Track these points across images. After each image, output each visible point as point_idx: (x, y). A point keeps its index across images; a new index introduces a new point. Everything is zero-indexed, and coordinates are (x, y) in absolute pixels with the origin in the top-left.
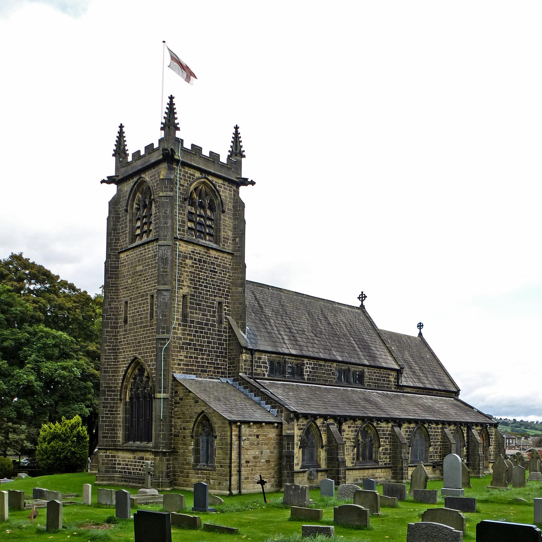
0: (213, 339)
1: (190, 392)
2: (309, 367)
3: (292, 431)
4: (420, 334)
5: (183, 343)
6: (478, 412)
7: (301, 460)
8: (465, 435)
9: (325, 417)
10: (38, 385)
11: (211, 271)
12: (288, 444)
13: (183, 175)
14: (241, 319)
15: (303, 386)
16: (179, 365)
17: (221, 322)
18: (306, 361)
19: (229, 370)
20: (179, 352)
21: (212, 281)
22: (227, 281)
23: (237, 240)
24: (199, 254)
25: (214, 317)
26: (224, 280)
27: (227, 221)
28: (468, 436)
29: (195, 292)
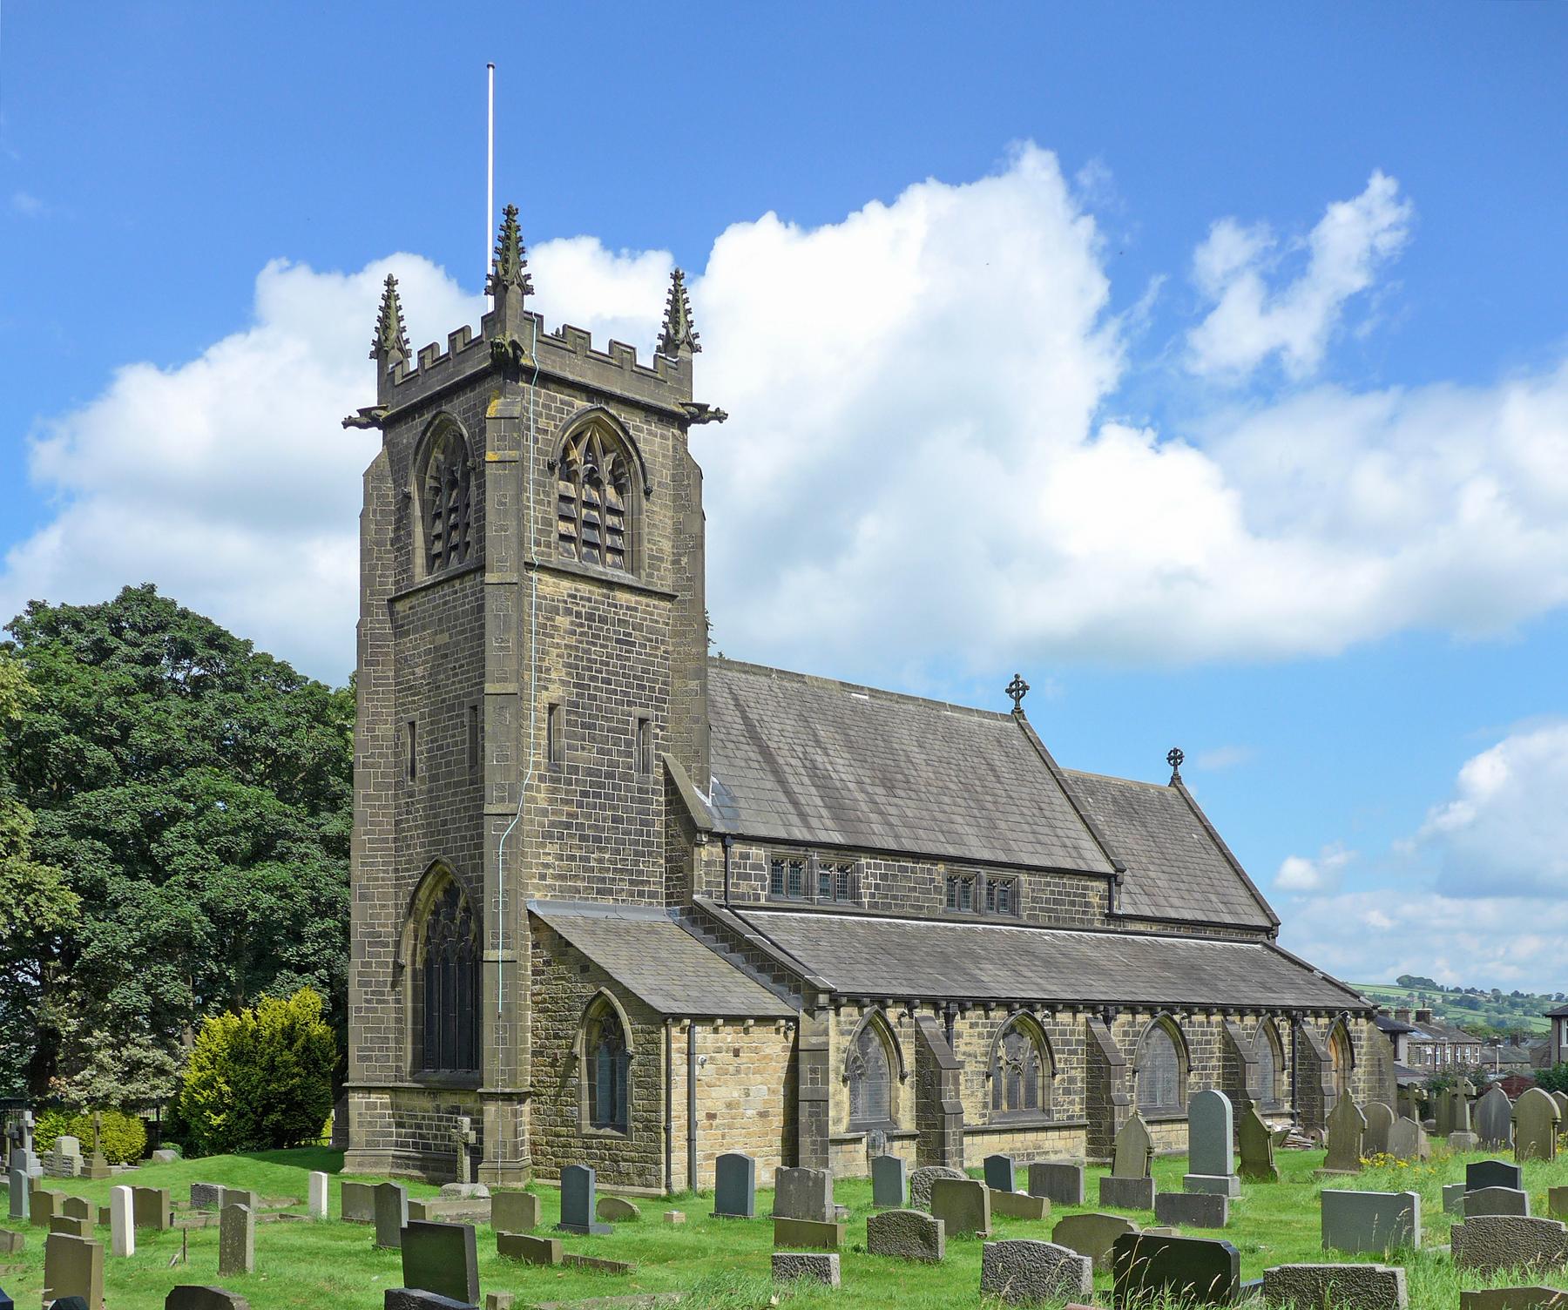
0: (626, 810)
1: (569, 944)
3: (823, 1039)
4: (1176, 780)
5: (553, 824)
6: (1326, 979)
7: (846, 1106)
9: (908, 1002)
10: (202, 928)
12: (814, 1071)
13: (544, 406)
14: (699, 756)
16: (543, 877)
17: (646, 769)
19: (667, 888)
20: (543, 845)
23: (684, 560)
24: (589, 600)
25: (630, 755)
27: (658, 516)
28: (1293, 1043)
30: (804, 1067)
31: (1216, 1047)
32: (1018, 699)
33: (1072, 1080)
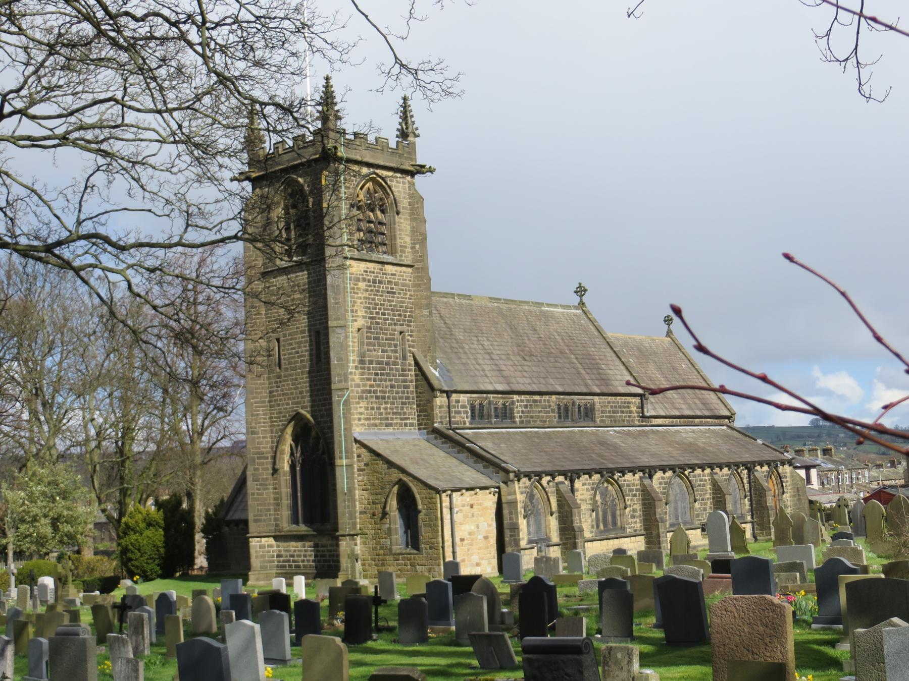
0: (396, 381)
2: (521, 406)
5: (363, 392)
8: (745, 481)
11: (388, 292)
12: (511, 513)
15: (517, 433)
16: (359, 419)
18: (516, 397)
19: (418, 420)
20: (358, 403)
21: (391, 306)
22: (408, 303)
23: (417, 246)
25: (396, 352)
26: (404, 302)
27: (403, 226)
28: (749, 482)
29: (372, 323)
30: (506, 512)
31: (708, 487)
32: (581, 296)
33: (635, 511)
